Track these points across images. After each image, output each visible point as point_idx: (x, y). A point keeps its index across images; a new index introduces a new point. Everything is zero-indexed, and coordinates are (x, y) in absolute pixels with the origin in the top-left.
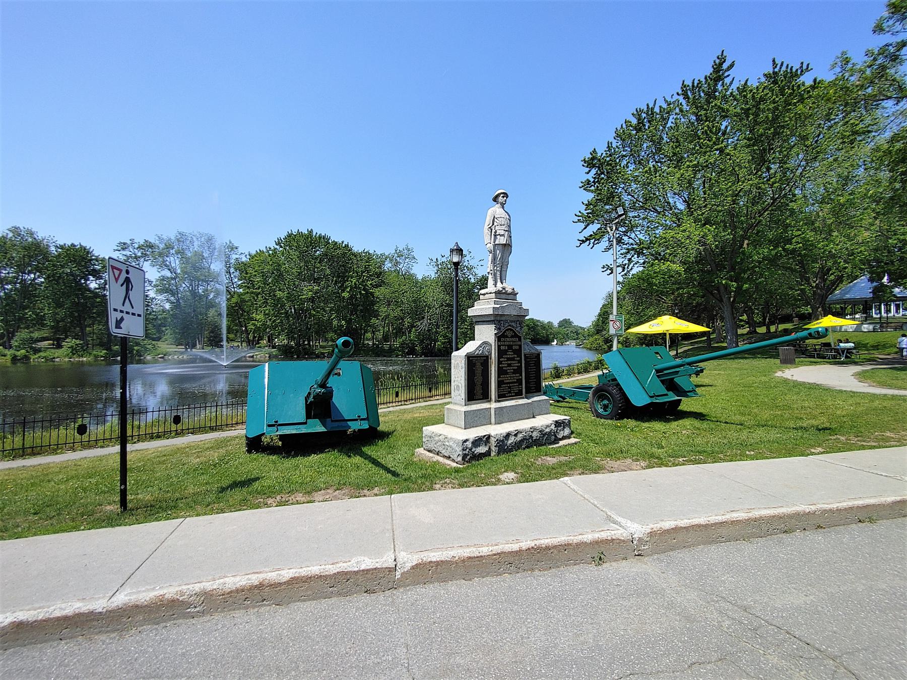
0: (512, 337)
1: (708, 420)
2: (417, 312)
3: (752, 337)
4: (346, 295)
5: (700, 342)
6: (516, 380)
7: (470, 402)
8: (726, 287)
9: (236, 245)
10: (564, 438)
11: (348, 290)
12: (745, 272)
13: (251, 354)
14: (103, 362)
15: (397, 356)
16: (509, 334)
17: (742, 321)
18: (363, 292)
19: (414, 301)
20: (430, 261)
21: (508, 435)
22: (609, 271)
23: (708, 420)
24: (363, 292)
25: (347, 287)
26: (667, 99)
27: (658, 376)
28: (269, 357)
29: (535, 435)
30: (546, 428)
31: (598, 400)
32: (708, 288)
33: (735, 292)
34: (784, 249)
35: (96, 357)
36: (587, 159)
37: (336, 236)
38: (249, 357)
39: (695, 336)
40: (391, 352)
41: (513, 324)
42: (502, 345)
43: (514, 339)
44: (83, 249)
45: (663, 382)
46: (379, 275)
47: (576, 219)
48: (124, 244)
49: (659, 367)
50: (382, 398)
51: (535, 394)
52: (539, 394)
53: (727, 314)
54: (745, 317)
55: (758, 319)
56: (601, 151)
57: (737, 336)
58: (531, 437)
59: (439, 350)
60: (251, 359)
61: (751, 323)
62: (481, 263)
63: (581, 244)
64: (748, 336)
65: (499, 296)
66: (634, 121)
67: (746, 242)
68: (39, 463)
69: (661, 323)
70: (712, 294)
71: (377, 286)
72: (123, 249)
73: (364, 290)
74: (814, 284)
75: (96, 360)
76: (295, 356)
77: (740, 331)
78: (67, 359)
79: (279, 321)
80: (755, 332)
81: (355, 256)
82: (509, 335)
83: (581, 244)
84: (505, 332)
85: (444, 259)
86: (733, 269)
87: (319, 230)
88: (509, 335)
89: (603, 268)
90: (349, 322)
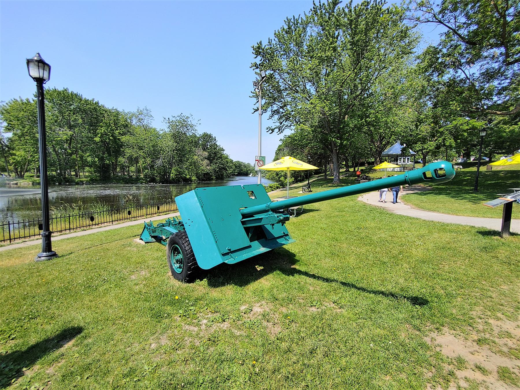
1: (300, 272)
2: (155, 153)
3: (347, 174)
4: (97, 139)
5: (322, 176)
8: (335, 144)
11: (99, 135)
12: (345, 134)
13: (15, 182)
15: (141, 183)
17: (343, 165)
18: (111, 138)
19: (153, 146)
20: (164, 119)
22: (271, 131)
23: (300, 272)
24: (111, 138)
26: (306, 14)
27: (243, 223)
28: (33, 184)
31: (174, 253)
32: (326, 144)
33: (340, 146)
34: (365, 121)
36: (255, 47)
37: (87, 95)
38: (13, 184)
40: (137, 181)
45: (247, 230)
46: (126, 126)
47: (252, 95)
49: (246, 211)
50: (78, 221)
53: (335, 160)
54: (344, 163)
55: (350, 164)
56: (265, 44)
57: (339, 173)
59: (173, 179)
60: (15, 186)
61: (347, 166)
62: (200, 122)
63: (255, 112)
64: (345, 173)
66: (286, 27)
67: (347, 116)
69: (283, 162)
70: (327, 147)
71: (124, 134)
73: (112, 136)
74: (377, 146)
76: (57, 184)
77: (341, 170)
80: (349, 171)
83: (255, 112)
85: (174, 119)
86: (339, 132)
87: (73, 89)
89: (267, 129)
90: (102, 159)
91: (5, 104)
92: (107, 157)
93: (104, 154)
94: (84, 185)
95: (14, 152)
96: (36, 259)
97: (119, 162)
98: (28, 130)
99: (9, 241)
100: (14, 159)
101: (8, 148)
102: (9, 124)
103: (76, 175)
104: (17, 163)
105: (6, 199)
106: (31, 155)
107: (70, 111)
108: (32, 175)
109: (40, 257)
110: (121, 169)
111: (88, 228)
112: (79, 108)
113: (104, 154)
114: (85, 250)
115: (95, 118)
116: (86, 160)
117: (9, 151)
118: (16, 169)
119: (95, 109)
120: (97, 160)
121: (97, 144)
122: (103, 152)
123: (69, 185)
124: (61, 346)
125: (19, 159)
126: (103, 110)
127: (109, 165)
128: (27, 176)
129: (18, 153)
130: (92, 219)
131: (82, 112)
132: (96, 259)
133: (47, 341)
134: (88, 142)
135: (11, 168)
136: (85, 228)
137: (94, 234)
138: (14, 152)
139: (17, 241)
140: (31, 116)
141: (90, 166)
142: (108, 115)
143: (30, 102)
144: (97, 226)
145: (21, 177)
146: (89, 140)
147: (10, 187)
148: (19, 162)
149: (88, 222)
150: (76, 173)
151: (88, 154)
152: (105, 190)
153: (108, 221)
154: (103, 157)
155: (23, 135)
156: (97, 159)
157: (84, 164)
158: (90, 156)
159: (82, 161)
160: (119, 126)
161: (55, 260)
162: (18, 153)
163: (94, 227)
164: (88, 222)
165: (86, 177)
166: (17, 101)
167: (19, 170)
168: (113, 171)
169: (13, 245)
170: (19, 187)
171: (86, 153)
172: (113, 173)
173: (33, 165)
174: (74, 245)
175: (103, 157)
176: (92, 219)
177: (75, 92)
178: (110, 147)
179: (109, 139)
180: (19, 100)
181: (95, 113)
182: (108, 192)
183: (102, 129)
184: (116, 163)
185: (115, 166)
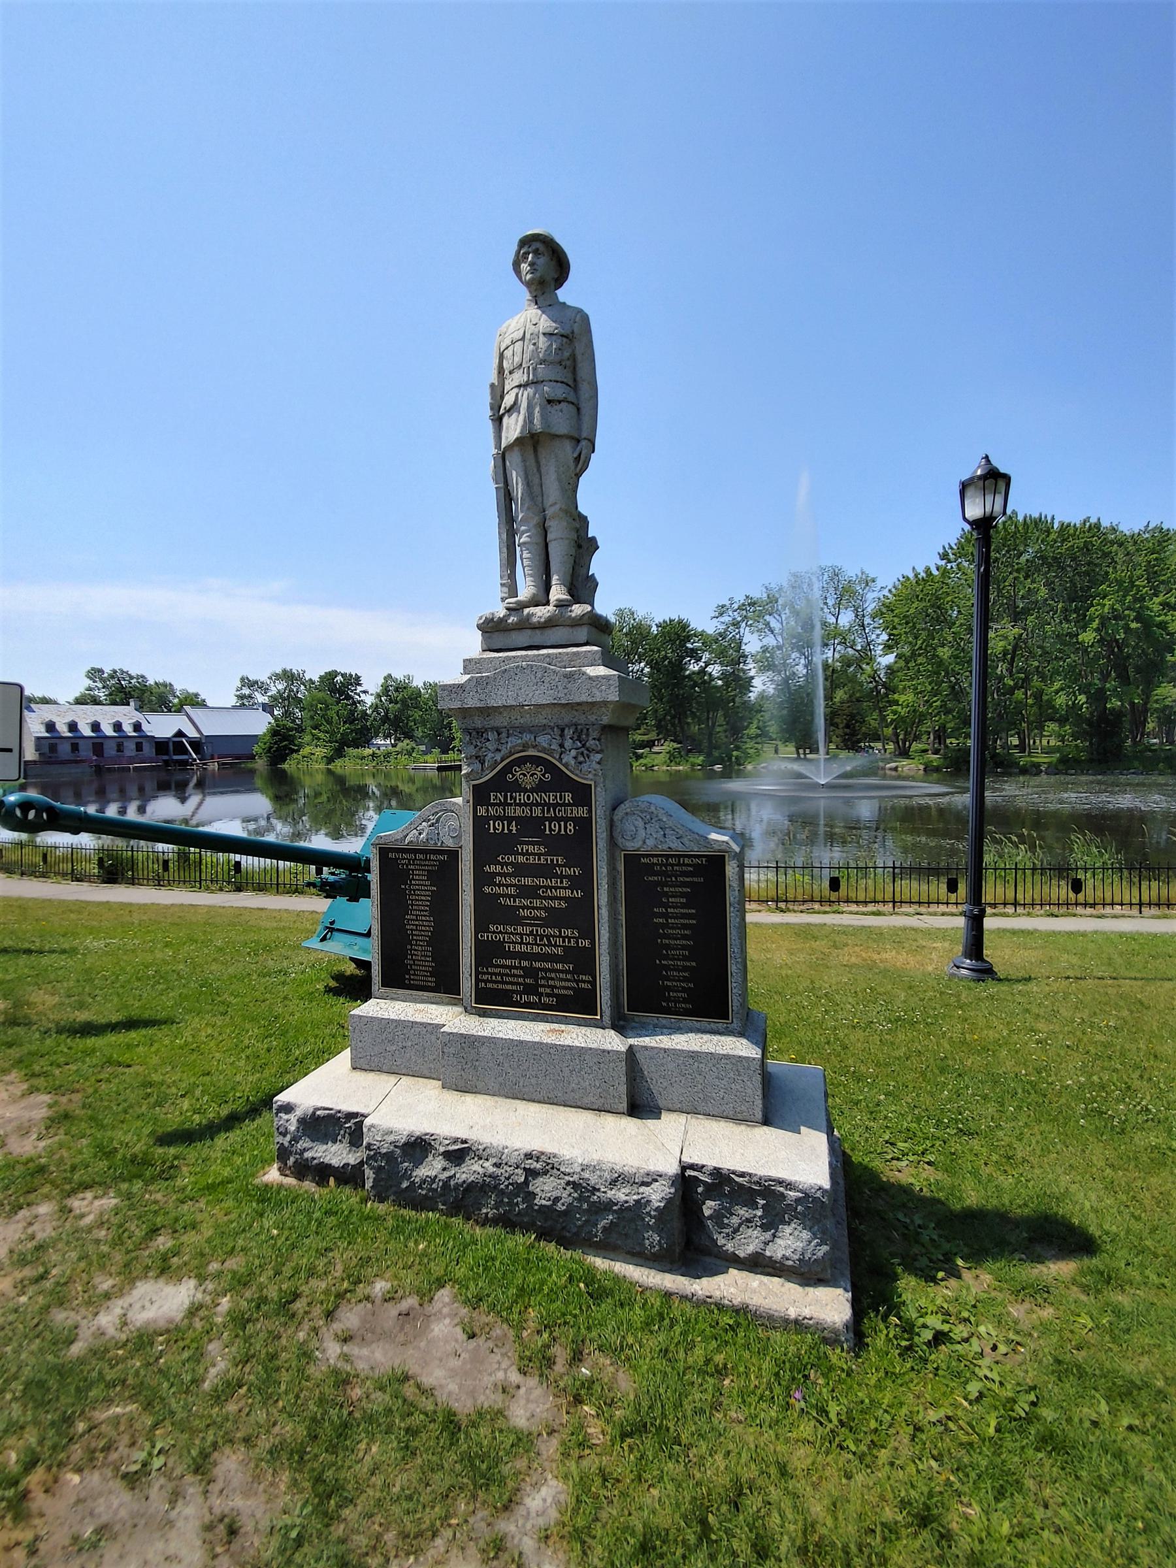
0: (541, 787)
4: (1088, 637)
6: (560, 951)
7: (388, 990)
9: (872, 576)
10: (758, 1264)
11: (1095, 625)
13: (893, 765)
14: (700, 773)
16: (528, 777)
18: (1134, 625)
21: (418, 1147)
25: (1092, 620)
28: (925, 770)
29: (546, 1189)
30: (613, 1183)
35: (693, 765)
38: (890, 769)
39: (583, 1022)
41: (543, 740)
42: (495, 819)
43: (550, 798)
44: (680, 622)
48: (723, 606)
51: (690, 1021)
52: (720, 1024)
58: (523, 1190)
60: (894, 773)
65: (499, 640)
68: (311, 908)
72: (721, 614)
75: (693, 770)
78: (665, 768)
79: (938, 703)
81: (1121, 545)
82: (528, 782)
84: (508, 769)
88: (528, 782)
90: (1099, 697)
91: (887, 594)
92: (1115, 690)
93: (1105, 677)
94: (1044, 776)
95: (896, 696)
96: (948, 969)
97: (1157, 701)
98: (924, 641)
99: (891, 905)
100: (895, 713)
101: (886, 688)
102: (890, 635)
103: (1022, 747)
104: (899, 722)
105: (875, 804)
106: (927, 701)
107: (1018, 571)
108: (926, 747)
109: (958, 967)
110: (1160, 724)
111: (1063, 910)
112: (1041, 558)
113: (1105, 677)
114: (1065, 983)
115: (1087, 573)
116: (1049, 701)
117: (886, 695)
118: (897, 735)
119: (1087, 548)
120: (1084, 700)
121: (1085, 651)
122: (1102, 672)
123: (1003, 774)
124: (1040, 1260)
125: (903, 712)
126: (1112, 543)
127: (1118, 714)
128: (916, 751)
129: (902, 698)
130: (1077, 886)
131: (1050, 566)
132: (1107, 1026)
133: (1001, 1218)
134: (1060, 651)
135: (889, 731)
136: (1055, 909)
137: (1084, 934)
138: (896, 696)
139: (906, 909)
140: (932, 606)
141: (1062, 721)
142: (1128, 554)
143: (931, 574)
144: (1089, 911)
145: (904, 753)
146: (1064, 643)
147: (884, 777)
148: (902, 719)
149: (1063, 892)
150: (1022, 741)
151: (1057, 685)
152: (1112, 793)
153: (1126, 900)
154: (1102, 691)
155: (914, 655)
156: (1082, 698)
157: (1046, 712)
158: (1062, 689)
159: (1040, 707)
160: (1163, 582)
161: (992, 988)
162: (902, 698)
163: (1080, 910)
164: (1063, 891)
165: (1049, 751)
166: (908, 579)
167: (901, 737)
168: (1131, 732)
169: (899, 917)
170: (899, 778)
171: (1052, 683)
172: (1134, 739)
173: (927, 726)
174: (1031, 956)
175: (1102, 691)
176: (1077, 886)
177: (1036, 515)
178: (1129, 656)
179: (1127, 629)
180: (911, 576)
181: (1083, 560)
182: (1125, 801)
183: (1106, 601)
184: (1146, 703)
185: (1139, 715)
